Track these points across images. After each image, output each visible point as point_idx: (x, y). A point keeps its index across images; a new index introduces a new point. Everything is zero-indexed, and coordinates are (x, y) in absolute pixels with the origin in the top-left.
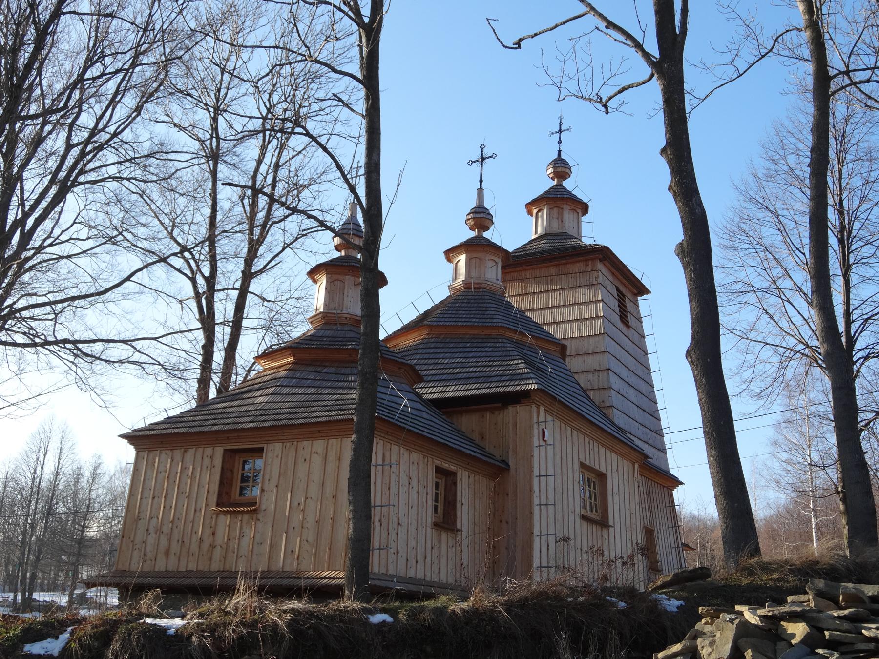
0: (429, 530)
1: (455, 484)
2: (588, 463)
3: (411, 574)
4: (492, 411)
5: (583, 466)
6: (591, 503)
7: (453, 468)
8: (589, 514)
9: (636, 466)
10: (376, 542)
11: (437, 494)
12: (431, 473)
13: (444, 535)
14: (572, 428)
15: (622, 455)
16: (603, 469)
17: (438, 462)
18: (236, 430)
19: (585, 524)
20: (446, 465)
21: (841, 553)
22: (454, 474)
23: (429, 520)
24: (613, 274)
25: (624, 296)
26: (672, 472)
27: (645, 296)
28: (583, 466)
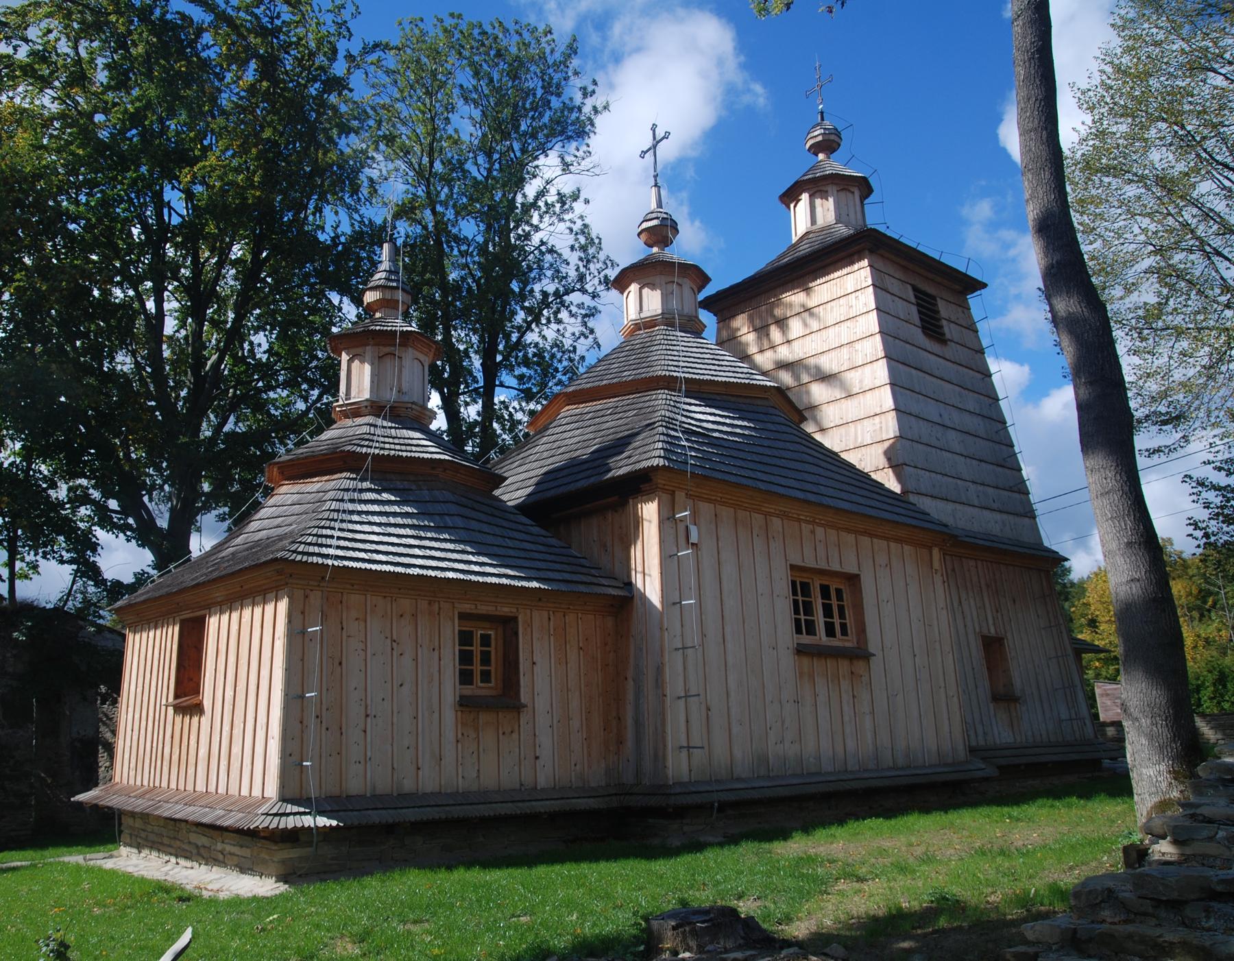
1: (516, 634)
2: (810, 563)
6: (842, 615)
9: (936, 551)
15: (899, 540)
16: (852, 569)
19: (806, 661)
25: (934, 298)
26: (1046, 544)
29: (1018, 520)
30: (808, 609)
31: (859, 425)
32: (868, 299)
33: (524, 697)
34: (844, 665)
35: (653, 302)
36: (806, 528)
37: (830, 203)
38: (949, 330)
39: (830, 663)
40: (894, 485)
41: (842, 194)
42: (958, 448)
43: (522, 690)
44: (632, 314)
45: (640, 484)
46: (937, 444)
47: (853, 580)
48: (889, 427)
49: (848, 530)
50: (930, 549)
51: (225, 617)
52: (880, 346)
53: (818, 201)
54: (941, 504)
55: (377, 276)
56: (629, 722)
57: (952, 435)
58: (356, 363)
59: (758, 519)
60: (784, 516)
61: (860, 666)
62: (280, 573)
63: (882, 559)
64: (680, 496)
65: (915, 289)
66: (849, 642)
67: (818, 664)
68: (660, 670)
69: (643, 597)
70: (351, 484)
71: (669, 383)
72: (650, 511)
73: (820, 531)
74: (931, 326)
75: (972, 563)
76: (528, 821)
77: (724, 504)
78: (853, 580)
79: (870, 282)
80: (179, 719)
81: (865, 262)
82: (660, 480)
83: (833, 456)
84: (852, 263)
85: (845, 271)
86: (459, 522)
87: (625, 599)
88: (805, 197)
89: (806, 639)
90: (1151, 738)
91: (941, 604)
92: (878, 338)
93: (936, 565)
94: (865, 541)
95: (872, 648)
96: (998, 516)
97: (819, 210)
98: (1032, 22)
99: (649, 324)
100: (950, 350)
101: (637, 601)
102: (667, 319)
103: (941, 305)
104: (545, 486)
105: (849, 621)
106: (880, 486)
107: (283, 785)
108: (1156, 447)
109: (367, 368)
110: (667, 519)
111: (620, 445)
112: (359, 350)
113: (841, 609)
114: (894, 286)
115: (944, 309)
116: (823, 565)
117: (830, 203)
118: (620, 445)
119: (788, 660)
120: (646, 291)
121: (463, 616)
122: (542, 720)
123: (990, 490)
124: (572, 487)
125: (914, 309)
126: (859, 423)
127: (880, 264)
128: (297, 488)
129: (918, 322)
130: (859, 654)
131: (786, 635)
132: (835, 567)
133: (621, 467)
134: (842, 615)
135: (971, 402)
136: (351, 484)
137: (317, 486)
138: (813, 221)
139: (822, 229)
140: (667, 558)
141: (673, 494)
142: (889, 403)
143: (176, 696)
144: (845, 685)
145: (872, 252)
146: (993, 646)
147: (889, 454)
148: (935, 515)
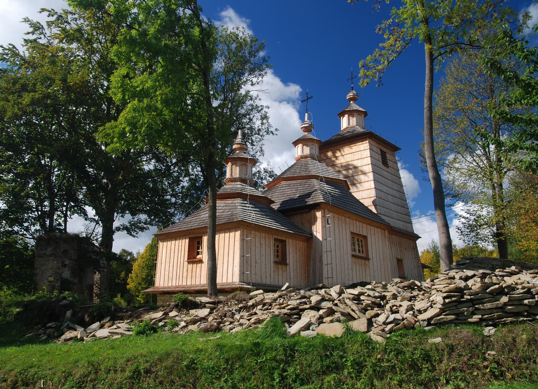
0: (272, 264)
1: (286, 245)
2: (355, 232)
3: (264, 282)
4: (306, 213)
5: (352, 233)
6: (362, 248)
7: (284, 238)
8: (357, 253)
9: (386, 231)
10: (325, 262)
11: (278, 250)
12: (272, 242)
13: (280, 266)
14: (345, 217)
15: (377, 227)
16: (365, 234)
17: (276, 237)
18: (191, 229)
19: (354, 259)
20: (279, 238)
21: (369, 287)
22: (285, 241)
23: (272, 261)
24: (377, 143)
25: (385, 153)
26: (415, 232)
27: (398, 151)
28: (352, 233)
29: (407, 224)
30: (354, 246)
31: (363, 192)
32: (368, 153)
33: (288, 262)
34: (363, 261)
35: (307, 151)
36: (355, 222)
37: (355, 119)
38: (390, 163)
39: (360, 260)
40: (374, 211)
41: (359, 116)
42: (391, 201)
43: (36, 348)
44: (300, 153)
45: (317, 206)
46: (386, 199)
47: (365, 237)
48: (373, 193)
49: (365, 223)
50: (385, 230)
51: (180, 241)
52: (371, 168)
53: (351, 118)
54: (389, 219)
55: (237, 140)
56: (311, 271)
57: (390, 196)
58: (234, 166)
59: (343, 218)
60: (349, 218)
61: (367, 262)
62: (238, 224)
63: (373, 232)
64: (326, 210)
65: (381, 150)
66: (364, 255)
67: (357, 260)
68: (321, 257)
69: (316, 237)
70: (242, 202)
71: (316, 177)
72: (319, 214)
73: (358, 223)
74: (385, 162)
75: (394, 236)
76: (399, 232)
77: (336, 213)
78: (365, 237)
79: (368, 148)
80: (190, 266)
81: (367, 142)
82: (322, 206)
83: (358, 201)
84: (363, 141)
85: (361, 143)
86: (270, 214)
87: (310, 238)
88: (346, 116)
89: (354, 253)
90: (445, 263)
91: (387, 247)
92: (370, 165)
93: (386, 235)
94: (369, 226)
95: (370, 257)
96: (402, 223)
97: (351, 120)
98: (429, 110)
99: (306, 157)
100: (390, 170)
101: (314, 238)
102: (312, 157)
103: (388, 155)
104: (284, 205)
105: (364, 249)
106: (371, 211)
107: (240, 278)
108: (428, 312)
109: (238, 168)
110: (323, 216)
111: (309, 195)
112: (235, 162)
113: (362, 245)
114: (375, 149)
115: (389, 156)
116: (358, 232)
117: (355, 119)
118: (309, 195)
119: (350, 257)
120: (305, 147)
121: (275, 239)
122: (292, 269)
123: (400, 215)
124: (290, 207)
125: (380, 156)
126: (365, 192)
127: (372, 142)
128: (223, 202)
129: (381, 160)
130: (367, 259)
131: (350, 252)
132: (361, 233)
133: (310, 201)
134: (362, 248)
135: (395, 187)
136: (242, 202)
137: (230, 202)
138: (349, 124)
139: (352, 127)
140: (323, 227)
141: (324, 210)
142: (373, 186)
143: (188, 259)
144: (363, 266)
145: (369, 138)
146: (399, 261)
147: (374, 202)
148: (386, 221)
